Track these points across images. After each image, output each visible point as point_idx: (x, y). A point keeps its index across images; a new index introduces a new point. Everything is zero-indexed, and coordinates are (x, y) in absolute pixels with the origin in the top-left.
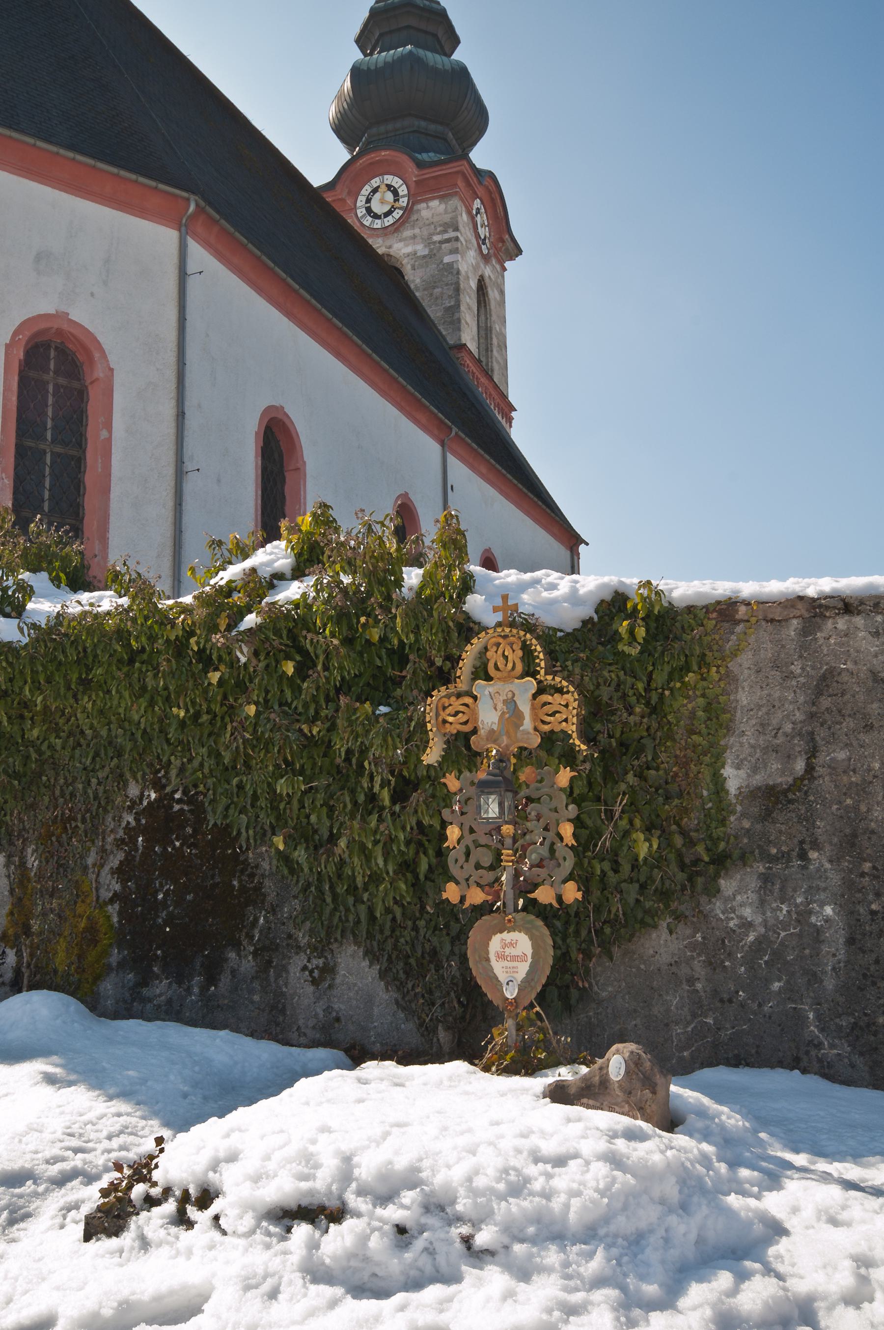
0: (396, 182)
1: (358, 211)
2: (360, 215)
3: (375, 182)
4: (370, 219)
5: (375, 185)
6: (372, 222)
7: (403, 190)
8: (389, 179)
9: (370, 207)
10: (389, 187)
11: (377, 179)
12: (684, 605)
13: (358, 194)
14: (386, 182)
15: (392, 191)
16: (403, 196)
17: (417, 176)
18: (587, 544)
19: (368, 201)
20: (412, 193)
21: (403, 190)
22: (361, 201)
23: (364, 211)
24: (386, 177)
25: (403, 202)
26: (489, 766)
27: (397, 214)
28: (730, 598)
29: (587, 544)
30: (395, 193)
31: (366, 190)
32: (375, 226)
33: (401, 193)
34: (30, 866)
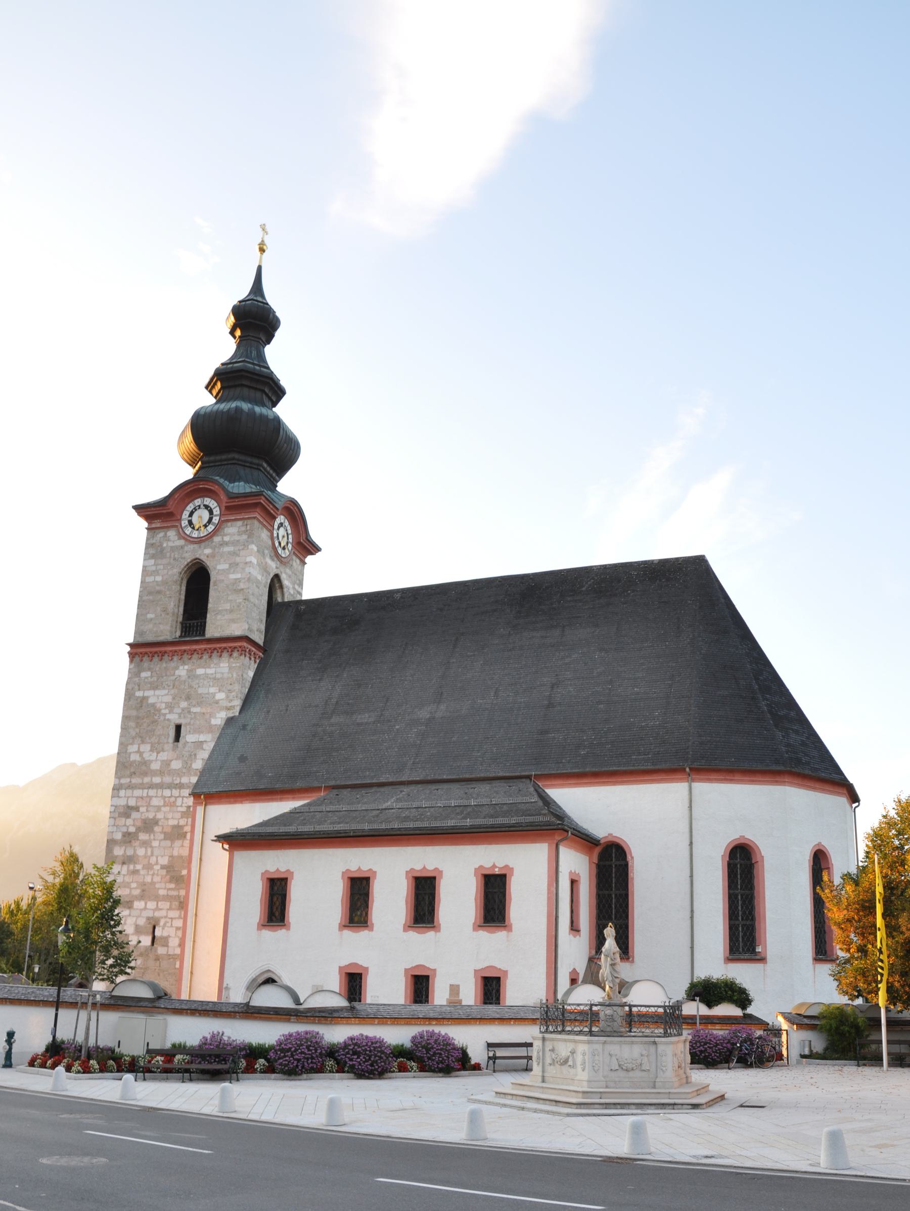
0: (212, 504)
1: (183, 522)
2: (183, 525)
3: (198, 502)
4: (190, 529)
5: (191, 510)
6: (191, 532)
7: (216, 511)
8: (208, 501)
9: (191, 520)
10: (206, 507)
11: (199, 500)
12: (886, 994)
13: (184, 509)
14: (205, 503)
15: (192, 524)
16: (216, 516)
17: (226, 503)
18: (213, 840)
19: (191, 514)
20: (222, 513)
21: (216, 511)
22: (186, 514)
23: (187, 523)
24: (206, 499)
25: (216, 520)
26: (67, 922)
27: (211, 528)
28: (746, 990)
29: (213, 840)
30: (211, 512)
31: (190, 507)
32: (193, 536)
33: (215, 513)
34: (727, 1032)
